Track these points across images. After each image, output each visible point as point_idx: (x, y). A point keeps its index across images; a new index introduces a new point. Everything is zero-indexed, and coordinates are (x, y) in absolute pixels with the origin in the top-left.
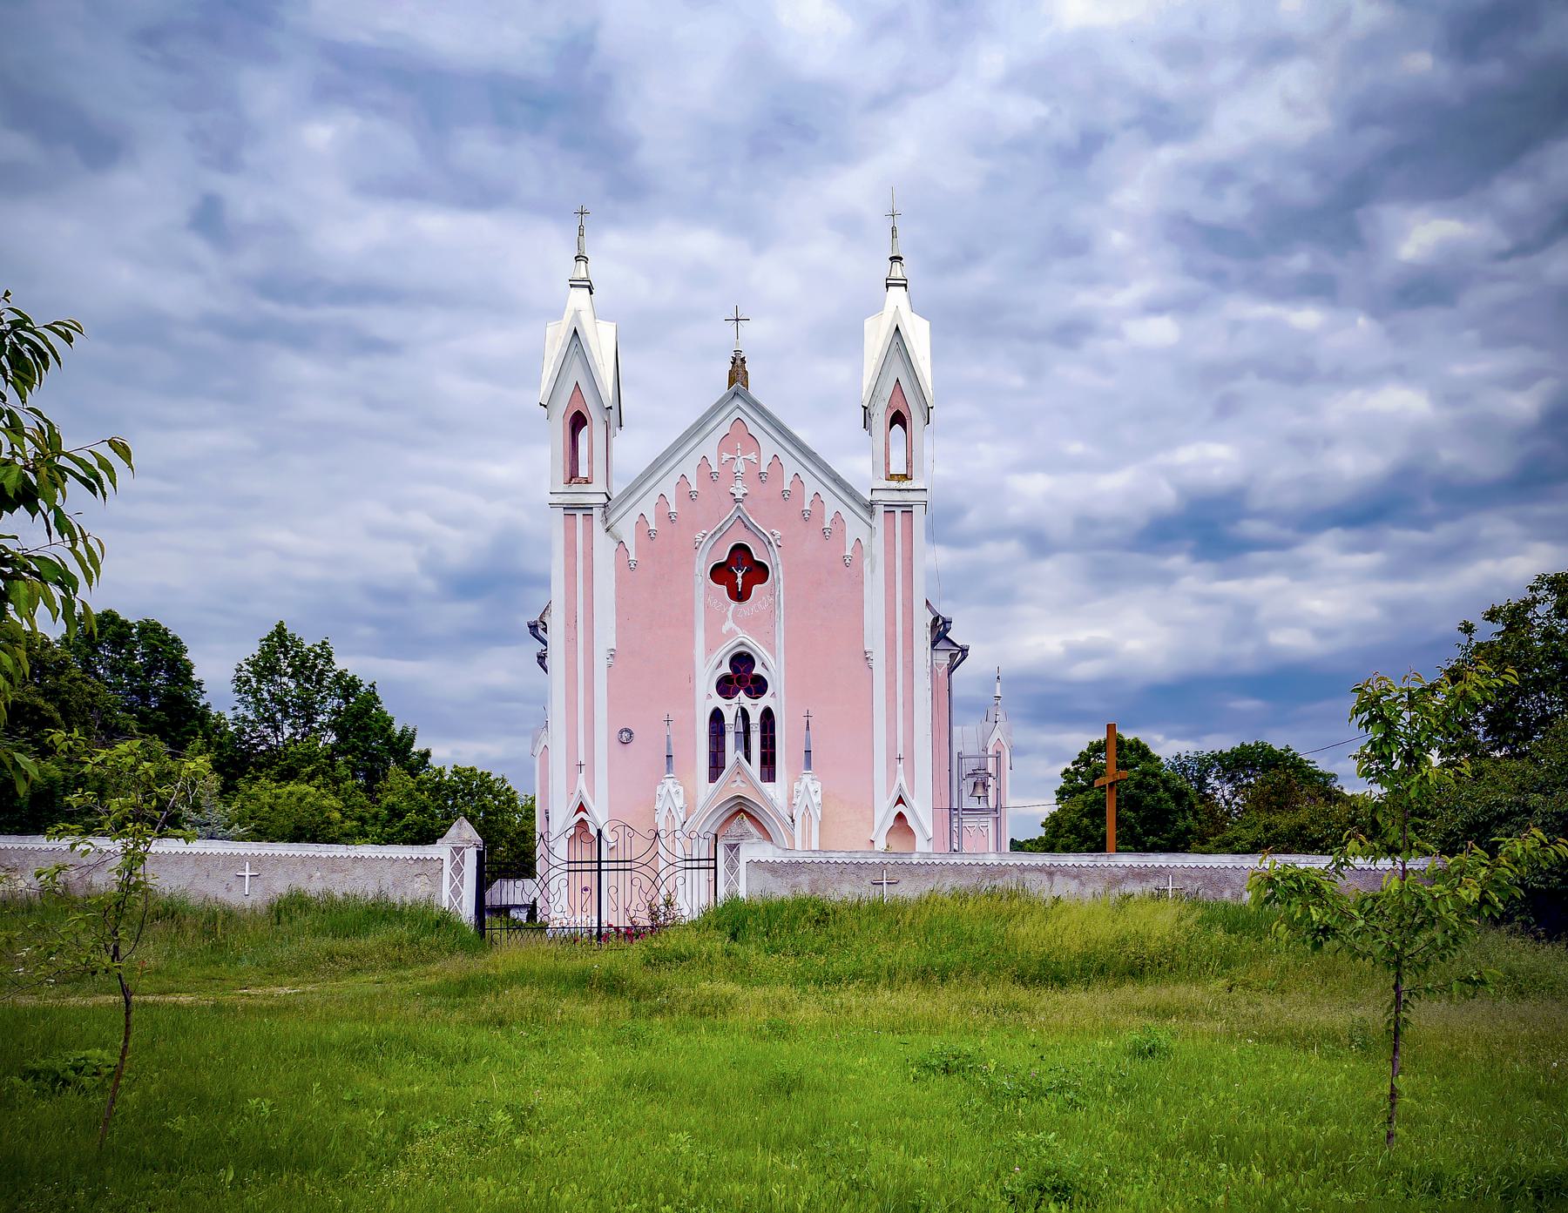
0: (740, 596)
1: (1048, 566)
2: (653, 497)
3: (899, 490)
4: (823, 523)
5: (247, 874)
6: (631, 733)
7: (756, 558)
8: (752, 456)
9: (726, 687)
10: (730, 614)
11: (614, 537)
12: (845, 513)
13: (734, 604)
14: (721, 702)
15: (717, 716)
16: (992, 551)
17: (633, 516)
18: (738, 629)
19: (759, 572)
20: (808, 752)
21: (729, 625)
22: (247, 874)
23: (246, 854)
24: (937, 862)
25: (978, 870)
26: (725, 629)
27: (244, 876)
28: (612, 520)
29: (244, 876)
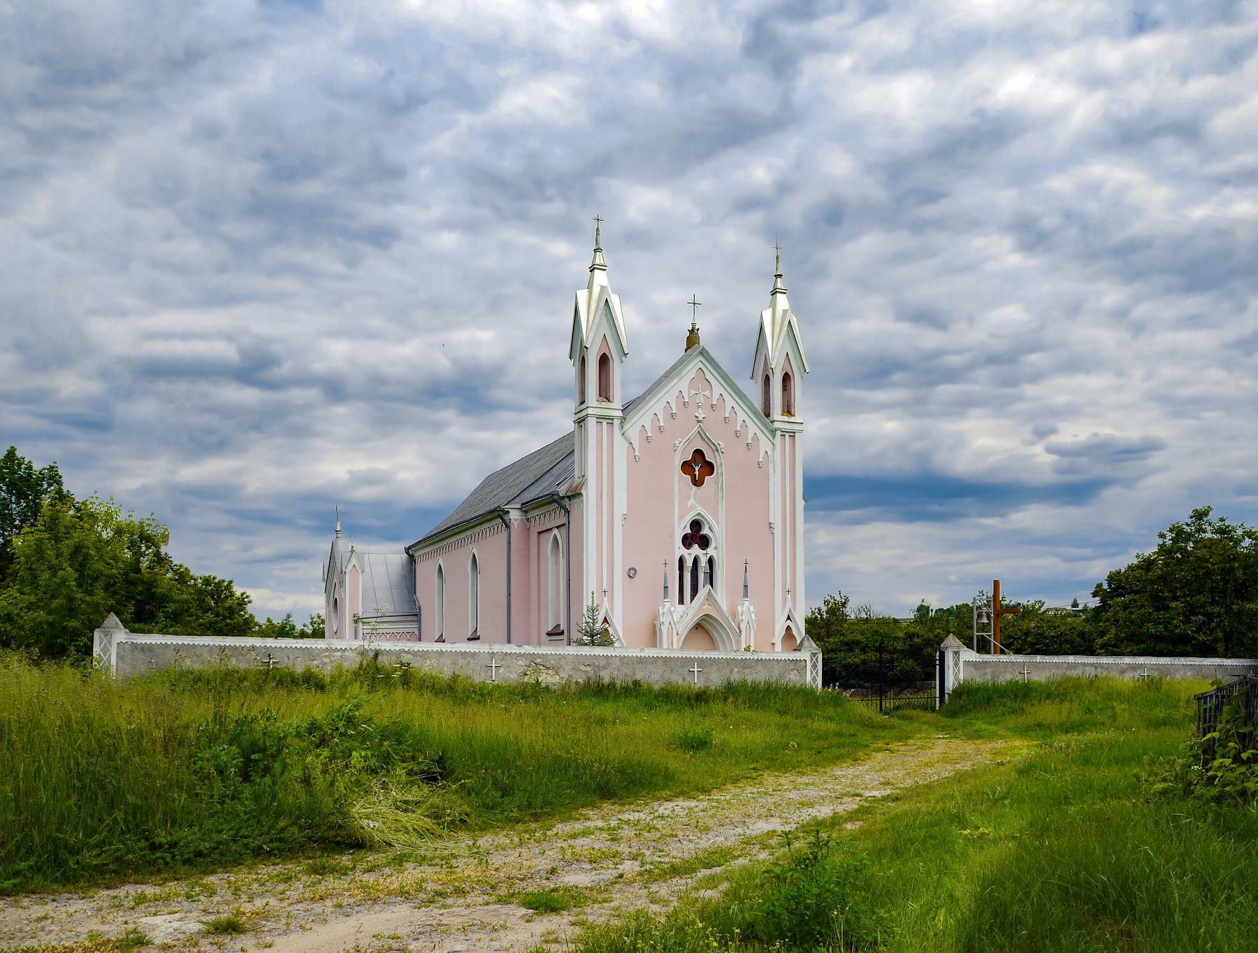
0: (697, 482)
1: (340, 410)
2: (650, 416)
3: (789, 422)
4: (747, 440)
5: (696, 670)
6: (636, 571)
7: (707, 459)
8: (707, 393)
9: (687, 541)
10: (692, 494)
11: (626, 439)
12: (760, 435)
13: (695, 488)
14: (684, 551)
15: (681, 561)
16: (297, 395)
17: (638, 427)
18: (697, 505)
19: (709, 468)
20: (746, 586)
21: (691, 501)
22: (696, 670)
23: (694, 657)
24: (1048, 661)
25: (1065, 665)
26: (689, 504)
27: (694, 671)
28: (626, 428)
29: (694, 671)
